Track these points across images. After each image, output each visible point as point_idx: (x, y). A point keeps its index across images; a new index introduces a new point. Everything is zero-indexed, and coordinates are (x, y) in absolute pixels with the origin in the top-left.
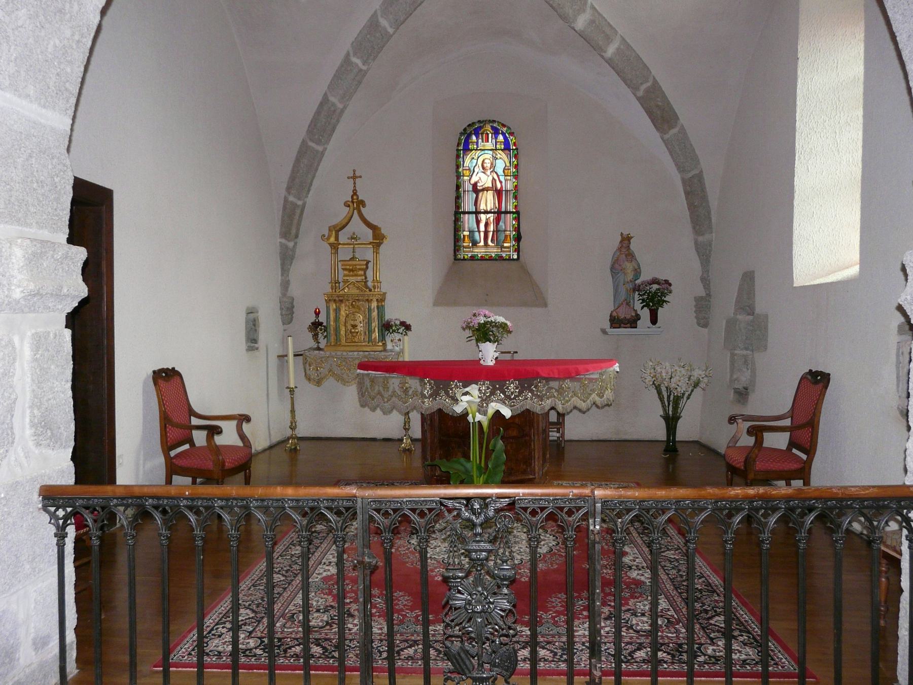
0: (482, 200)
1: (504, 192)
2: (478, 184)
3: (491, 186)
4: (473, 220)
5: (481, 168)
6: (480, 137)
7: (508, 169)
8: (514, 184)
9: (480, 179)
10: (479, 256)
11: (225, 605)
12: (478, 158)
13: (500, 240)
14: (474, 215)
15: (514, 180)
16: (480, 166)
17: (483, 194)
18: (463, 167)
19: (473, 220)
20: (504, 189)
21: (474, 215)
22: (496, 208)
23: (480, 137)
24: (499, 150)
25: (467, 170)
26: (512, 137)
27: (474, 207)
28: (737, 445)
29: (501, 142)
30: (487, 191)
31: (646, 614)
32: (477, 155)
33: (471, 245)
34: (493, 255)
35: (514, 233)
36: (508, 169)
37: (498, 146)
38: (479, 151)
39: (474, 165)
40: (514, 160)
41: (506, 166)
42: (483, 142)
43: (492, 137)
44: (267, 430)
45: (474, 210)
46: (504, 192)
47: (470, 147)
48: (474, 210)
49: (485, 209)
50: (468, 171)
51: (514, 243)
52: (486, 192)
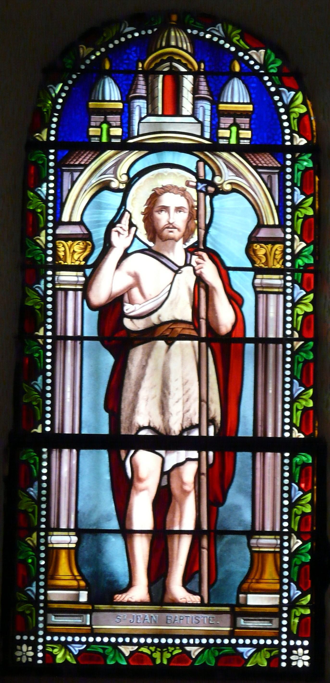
0: (146, 384)
1: (249, 348)
2: (128, 308)
3: (188, 316)
4: (97, 477)
5: (142, 233)
6: (142, 90)
7: (273, 241)
8: (301, 310)
9: (137, 283)
10: (126, 650)
11: (190, 51)
12: (130, 183)
13: (229, 574)
14: (104, 455)
15: (299, 293)
16: (138, 220)
17: (148, 355)
18: (58, 222)
19: (97, 477)
20: (250, 333)
21: (104, 455)
22: (211, 421)
23: (142, 90)
24: (229, 148)
25: (73, 238)
26: (288, 95)
27: (105, 416)
28: (257, 236)
29: (235, 114)
30: (170, 341)
31: (153, 112)
32: (123, 168)
33: (84, 596)
34: (195, 651)
35: (297, 543)
36: (273, 241)
37: (222, 133)
38: (135, 155)
39: (110, 215)
40: (299, 197)
41: (260, 225)
42: (152, 113)
43: (195, 90)
44: (94, 188)
45: (105, 430)
46: (249, 348)
47: (92, 131)
48: (105, 430)
49: (157, 423)
50: (78, 247)
51: (296, 593)
52: (161, 344)
